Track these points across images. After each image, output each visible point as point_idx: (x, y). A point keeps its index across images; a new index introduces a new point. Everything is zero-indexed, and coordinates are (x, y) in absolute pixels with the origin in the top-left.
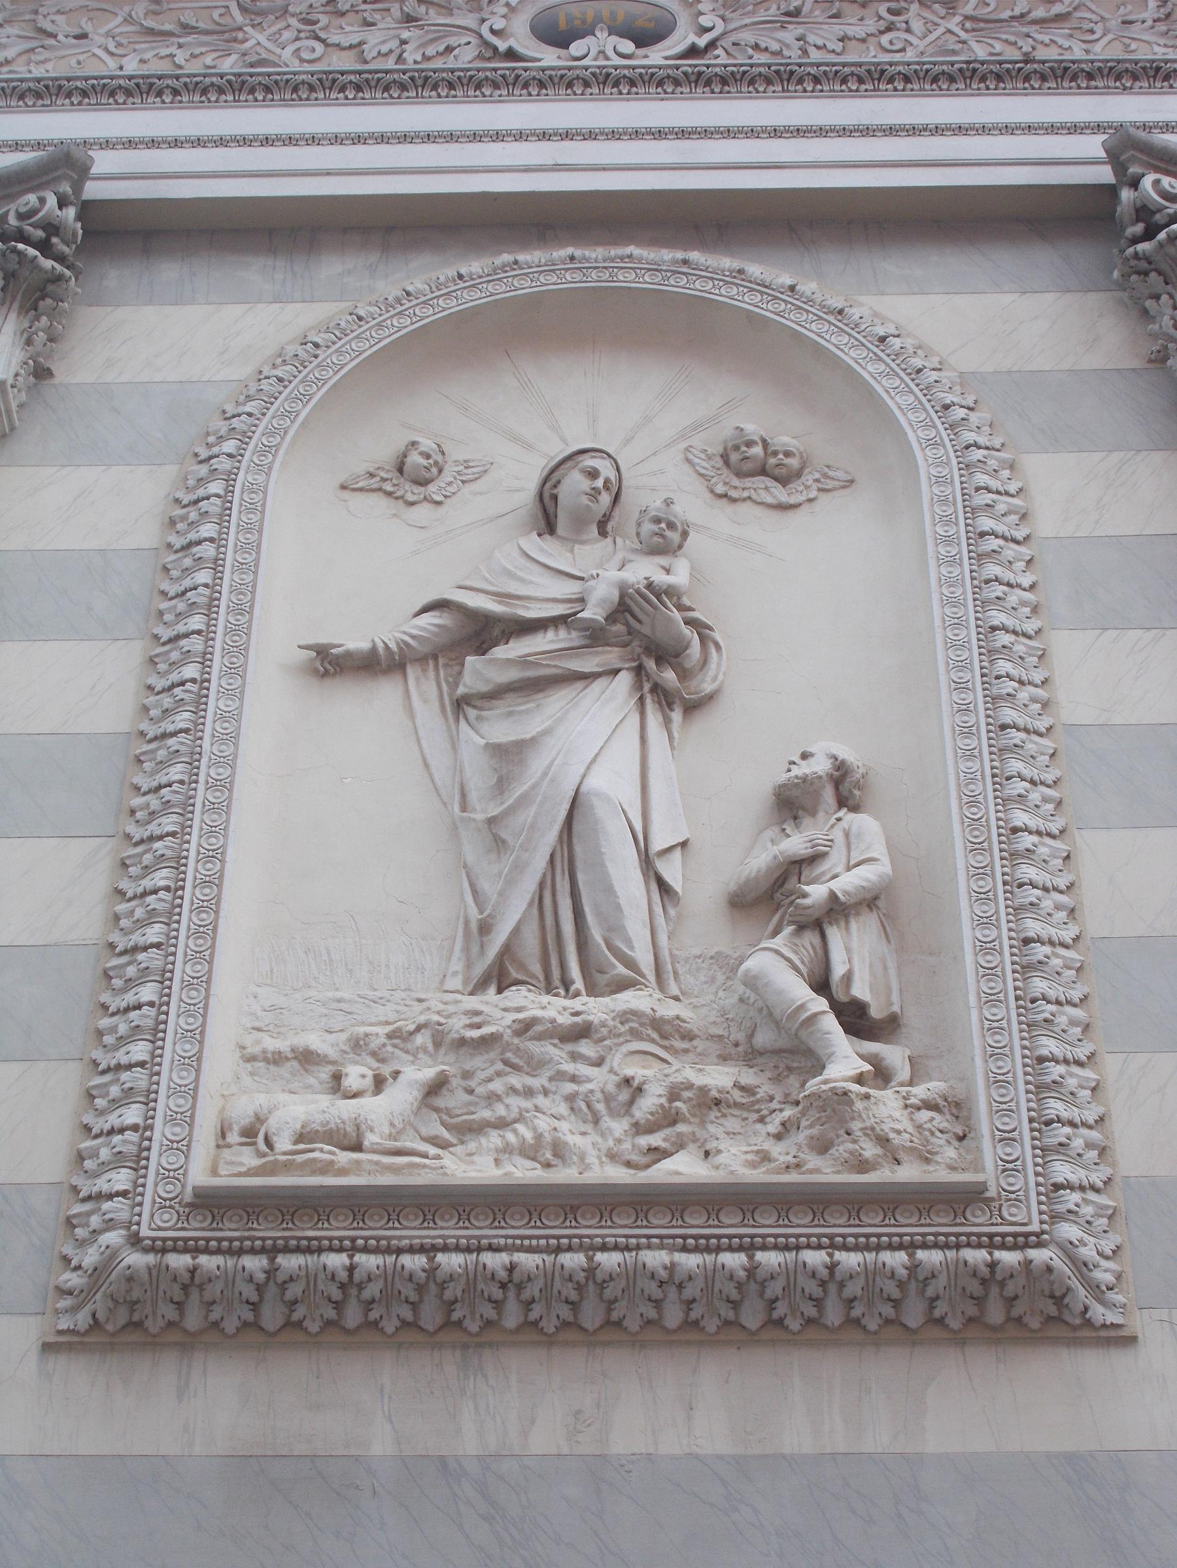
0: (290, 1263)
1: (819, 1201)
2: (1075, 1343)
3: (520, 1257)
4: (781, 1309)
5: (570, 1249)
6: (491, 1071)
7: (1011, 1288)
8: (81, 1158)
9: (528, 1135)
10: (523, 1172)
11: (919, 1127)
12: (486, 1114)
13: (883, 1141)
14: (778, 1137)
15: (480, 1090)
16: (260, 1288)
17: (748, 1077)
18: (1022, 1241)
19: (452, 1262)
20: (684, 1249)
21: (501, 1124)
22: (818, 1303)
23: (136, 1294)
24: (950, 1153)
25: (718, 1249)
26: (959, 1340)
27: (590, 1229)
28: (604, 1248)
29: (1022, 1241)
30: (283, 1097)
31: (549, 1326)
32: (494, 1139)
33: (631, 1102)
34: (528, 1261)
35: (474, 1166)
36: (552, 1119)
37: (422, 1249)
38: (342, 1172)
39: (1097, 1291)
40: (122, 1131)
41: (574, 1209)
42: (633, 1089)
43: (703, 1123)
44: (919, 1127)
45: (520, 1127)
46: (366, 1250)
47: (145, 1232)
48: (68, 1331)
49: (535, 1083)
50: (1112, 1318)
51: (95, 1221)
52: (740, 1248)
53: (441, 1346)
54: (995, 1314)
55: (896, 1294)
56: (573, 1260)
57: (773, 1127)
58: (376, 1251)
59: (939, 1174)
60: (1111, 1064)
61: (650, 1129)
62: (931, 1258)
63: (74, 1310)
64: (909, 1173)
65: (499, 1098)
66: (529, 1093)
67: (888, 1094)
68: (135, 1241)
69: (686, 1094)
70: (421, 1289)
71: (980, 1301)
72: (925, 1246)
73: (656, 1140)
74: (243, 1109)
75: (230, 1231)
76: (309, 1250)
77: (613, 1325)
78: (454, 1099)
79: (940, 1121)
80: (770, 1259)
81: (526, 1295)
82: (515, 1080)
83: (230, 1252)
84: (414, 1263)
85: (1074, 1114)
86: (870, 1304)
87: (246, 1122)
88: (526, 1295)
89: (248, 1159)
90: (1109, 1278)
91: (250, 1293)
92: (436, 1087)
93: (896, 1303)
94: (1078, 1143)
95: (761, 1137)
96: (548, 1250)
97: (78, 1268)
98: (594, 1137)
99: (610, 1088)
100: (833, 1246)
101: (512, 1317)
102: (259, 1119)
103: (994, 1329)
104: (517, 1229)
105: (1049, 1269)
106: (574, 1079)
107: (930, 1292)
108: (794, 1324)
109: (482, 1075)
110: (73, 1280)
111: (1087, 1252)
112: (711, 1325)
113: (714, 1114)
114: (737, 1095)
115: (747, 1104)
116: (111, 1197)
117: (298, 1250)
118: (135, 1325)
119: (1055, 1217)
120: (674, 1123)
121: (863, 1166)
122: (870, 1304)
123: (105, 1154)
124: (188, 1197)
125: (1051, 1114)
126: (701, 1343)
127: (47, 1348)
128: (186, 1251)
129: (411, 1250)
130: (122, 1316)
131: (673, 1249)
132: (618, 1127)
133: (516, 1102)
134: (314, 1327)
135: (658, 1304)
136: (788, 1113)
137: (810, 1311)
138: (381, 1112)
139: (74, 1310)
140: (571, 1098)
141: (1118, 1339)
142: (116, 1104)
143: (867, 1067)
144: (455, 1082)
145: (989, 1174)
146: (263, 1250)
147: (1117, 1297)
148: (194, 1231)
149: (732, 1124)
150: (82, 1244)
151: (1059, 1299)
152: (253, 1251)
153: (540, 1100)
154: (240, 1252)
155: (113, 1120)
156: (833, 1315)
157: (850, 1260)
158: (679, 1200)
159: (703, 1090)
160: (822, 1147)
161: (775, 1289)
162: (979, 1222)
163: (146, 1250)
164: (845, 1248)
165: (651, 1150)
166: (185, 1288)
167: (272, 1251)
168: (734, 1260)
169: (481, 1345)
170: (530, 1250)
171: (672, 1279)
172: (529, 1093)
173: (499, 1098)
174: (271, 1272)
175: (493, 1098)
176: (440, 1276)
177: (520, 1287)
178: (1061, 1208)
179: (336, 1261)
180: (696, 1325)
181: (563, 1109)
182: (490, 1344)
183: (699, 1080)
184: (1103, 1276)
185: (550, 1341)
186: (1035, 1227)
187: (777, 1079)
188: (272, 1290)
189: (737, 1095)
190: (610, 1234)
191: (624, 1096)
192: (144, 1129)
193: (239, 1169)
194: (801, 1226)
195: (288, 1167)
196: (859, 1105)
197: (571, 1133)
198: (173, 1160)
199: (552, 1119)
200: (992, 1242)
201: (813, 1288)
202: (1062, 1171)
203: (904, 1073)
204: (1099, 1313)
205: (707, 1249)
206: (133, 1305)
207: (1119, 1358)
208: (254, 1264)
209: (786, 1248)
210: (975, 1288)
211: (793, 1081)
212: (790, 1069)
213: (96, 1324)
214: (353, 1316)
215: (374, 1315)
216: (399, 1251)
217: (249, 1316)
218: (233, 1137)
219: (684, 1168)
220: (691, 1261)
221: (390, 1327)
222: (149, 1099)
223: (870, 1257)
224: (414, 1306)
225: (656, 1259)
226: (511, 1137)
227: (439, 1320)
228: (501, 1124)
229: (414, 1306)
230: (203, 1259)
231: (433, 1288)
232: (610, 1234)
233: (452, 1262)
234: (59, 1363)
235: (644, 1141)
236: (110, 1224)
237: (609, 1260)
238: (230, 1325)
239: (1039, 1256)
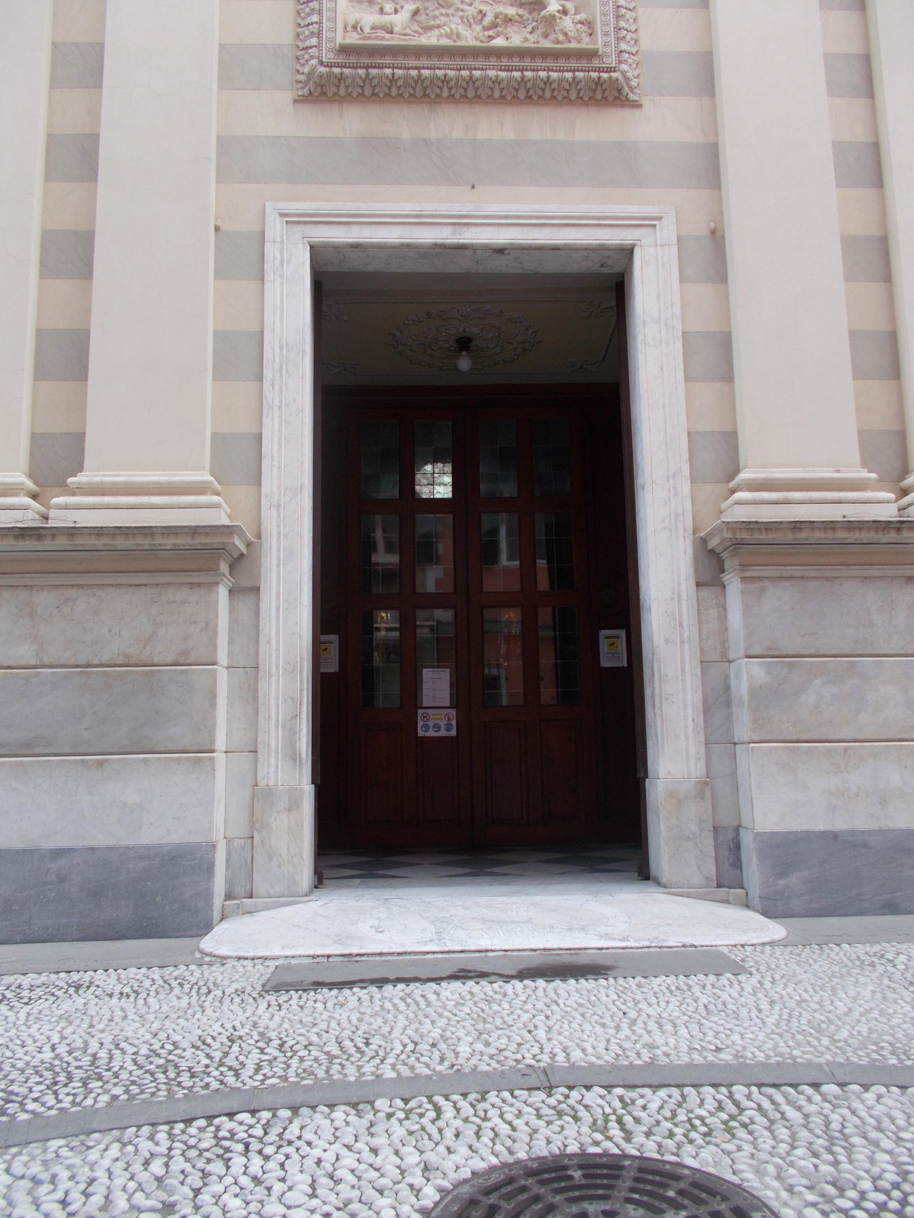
0: (373, 72)
1: (545, 54)
2: (622, 106)
3: (448, 72)
4: (531, 93)
5: (464, 69)
6: (434, 8)
7: (604, 86)
8: (298, 35)
9: (448, 30)
10: (445, 42)
11: (577, 30)
12: (433, 23)
13: (565, 34)
14: (531, 33)
15: (431, 14)
16: (364, 81)
17: (521, 12)
18: (610, 70)
19: (426, 73)
20: (501, 70)
21: (438, 27)
22: (543, 90)
23: (323, 82)
24: (587, 39)
25: (512, 70)
26: (586, 104)
27: (470, 62)
28: (475, 69)
29: (610, 70)
30: (364, 15)
31: (457, 97)
32: (436, 32)
33: (482, 20)
34: (451, 73)
35: (431, 39)
36: (455, 25)
37: (416, 68)
38: (387, 40)
39: (631, 88)
40: (312, 24)
41: (465, 55)
42: (482, 14)
43: (506, 27)
44: (577, 30)
45: (445, 28)
46: (397, 68)
47: (324, 60)
48: (302, 96)
49: (450, 11)
50: (635, 98)
51: (307, 57)
52: (519, 70)
53: (421, 103)
54: (599, 96)
55: (568, 87)
56: (465, 73)
57: (529, 29)
58: (401, 68)
59: (582, 46)
60: (640, 11)
61: (489, 29)
62: (580, 75)
63: (303, 88)
64: (574, 45)
65: (437, 17)
66: (447, 15)
67: (567, 18)
68: (321, 63)
69: (501, 16)
70: (416, 82)
71: (594, 91)
72: (578, 71)
73: (491, 33)
74: (352, 19)
75: (353, 60)
76: (379, 68)
77: (374, 94)
78: (422, 17)
79: (584, 28)
80: (529, 74)
81: (450, 85)
82: (443, 11)
83: (353, 68)
84: (414, 73)
85: (628, 27)
86: (559, 91)
87: (353, 23)
88: (450, 85)
89: (355, 35)
90: (635, 85)
91: (360, 82)
92: (416, 13)
93: (568, 91)
94: (628, 37)
95: (525, 33)
96: (457, 69)
97: (303, 73)
98: (469, 31)
99: (475, 14)
100: (549, 70)
101: (445, 93)
102: (357, 23)
103: (598, 101)
104: (446, 62)
105: (617, 80)
106: (462, 10)
107: (579, 87)
108: (535, 98)
109: (431, 9)
110: (302, 78)
111: (629, 75)
112: (509, 97)
113: (509, 24)
114: (517, 18)
115: (520, 22)
116: (311, 47)
117: (375, 67)
118: (324, 94)
119: (620, 62)
120: (496, 27)
121: (558, 42)
122: (559, 91)
123: (307, 33)
124: (337, 48)
125: (621, 26)
126: (505, 104)
127: (296, 101)
128: (338, 67)
129: (413, 68)
130: (319, 91)
131: (497, 70)
132: (478, 28)
133: (443, 19)
134: (381, 95)
135: (492, 89)
136: (534, 24)
137: (540, 93)
138: (400, 19)
139: (303, 88)
140: (462, 17)
141: (636, 105)
142: (308, 15)
143: (561, 8)
144: (422, 11)
145: (600, 46)
146: (364, 67)
147: (637, 91)
148: (341, 59)
149: (515, 28)
150: (303, 65)
151: (619, 91)
152: (360, 67)
153: (451, 18)
154: (356, 68)
155: (308, 20)
156: (548, 95)
157: (554, 75)
158: (499, 53)
159: (506, 15)
160: (546, 36)
161: (529, 85)
162: (596, 63)
163: (325, 66)
164: (553, 71)
165: (489, 36)
166: (339, 80)
167: (367, 68)
168: (517, 74)
169: (435, 103)
170: (451, 69)
171: (497, 81)
172: (447, 15)
173: (437, 17)
174: (367, 75)
175: (435, 17)
176: (422, 78)
177: (448, 83)
178: (622, 59)
179: (388, 71)
180: (376, 95)
181: (459, 21)
182: (439, 102)
183: (505, 11)
184: (634, 83)
185: (457, 102)
186: (613, 65)
187: (530, 13)
188: (368, 82)
189: (517, 18)
190: (478, 64)
191: (480, 17)
192: (320, 23)
193: (353, 39)
194: (539, 63)
195: (369, 38)
196: (558, 21)
197: (462, 29)
198: (331, 35)
199: (455, 25)
200: (600, 70)
201: (542, 85)
202: (623, 46)
203: (572, 11)
204: (631, 96)
205: (508, 70)
206: (322, 86)
207: (637, 112)
208: (361, 72)
209: (534, 70)
210: (593, 86)
211: (535, 14)
212: (534, 9)
213: (311, 93)
214: (394, 92)
215: (401, 92)
216: (408, 69)
217: (360, 91)
218: (349, 28)
219: (499, 42)
220: (503, 74)
221: (406, 95)
222: (320, 13)
223: (561, 74)
224: (414, 89)
225: (492, 73)
226: (442, 31)
227: (422, 94)
228: (438, 27)
229: (414, 89)
230: (345, 70)
231: (420, 82)
232: (478, 64)
233: (426, 73)
234: (300, 106)
235: (487, 33)
236: (312, 57)
237: (477, 73)
238: (355, 94)
239: (615, 75)
